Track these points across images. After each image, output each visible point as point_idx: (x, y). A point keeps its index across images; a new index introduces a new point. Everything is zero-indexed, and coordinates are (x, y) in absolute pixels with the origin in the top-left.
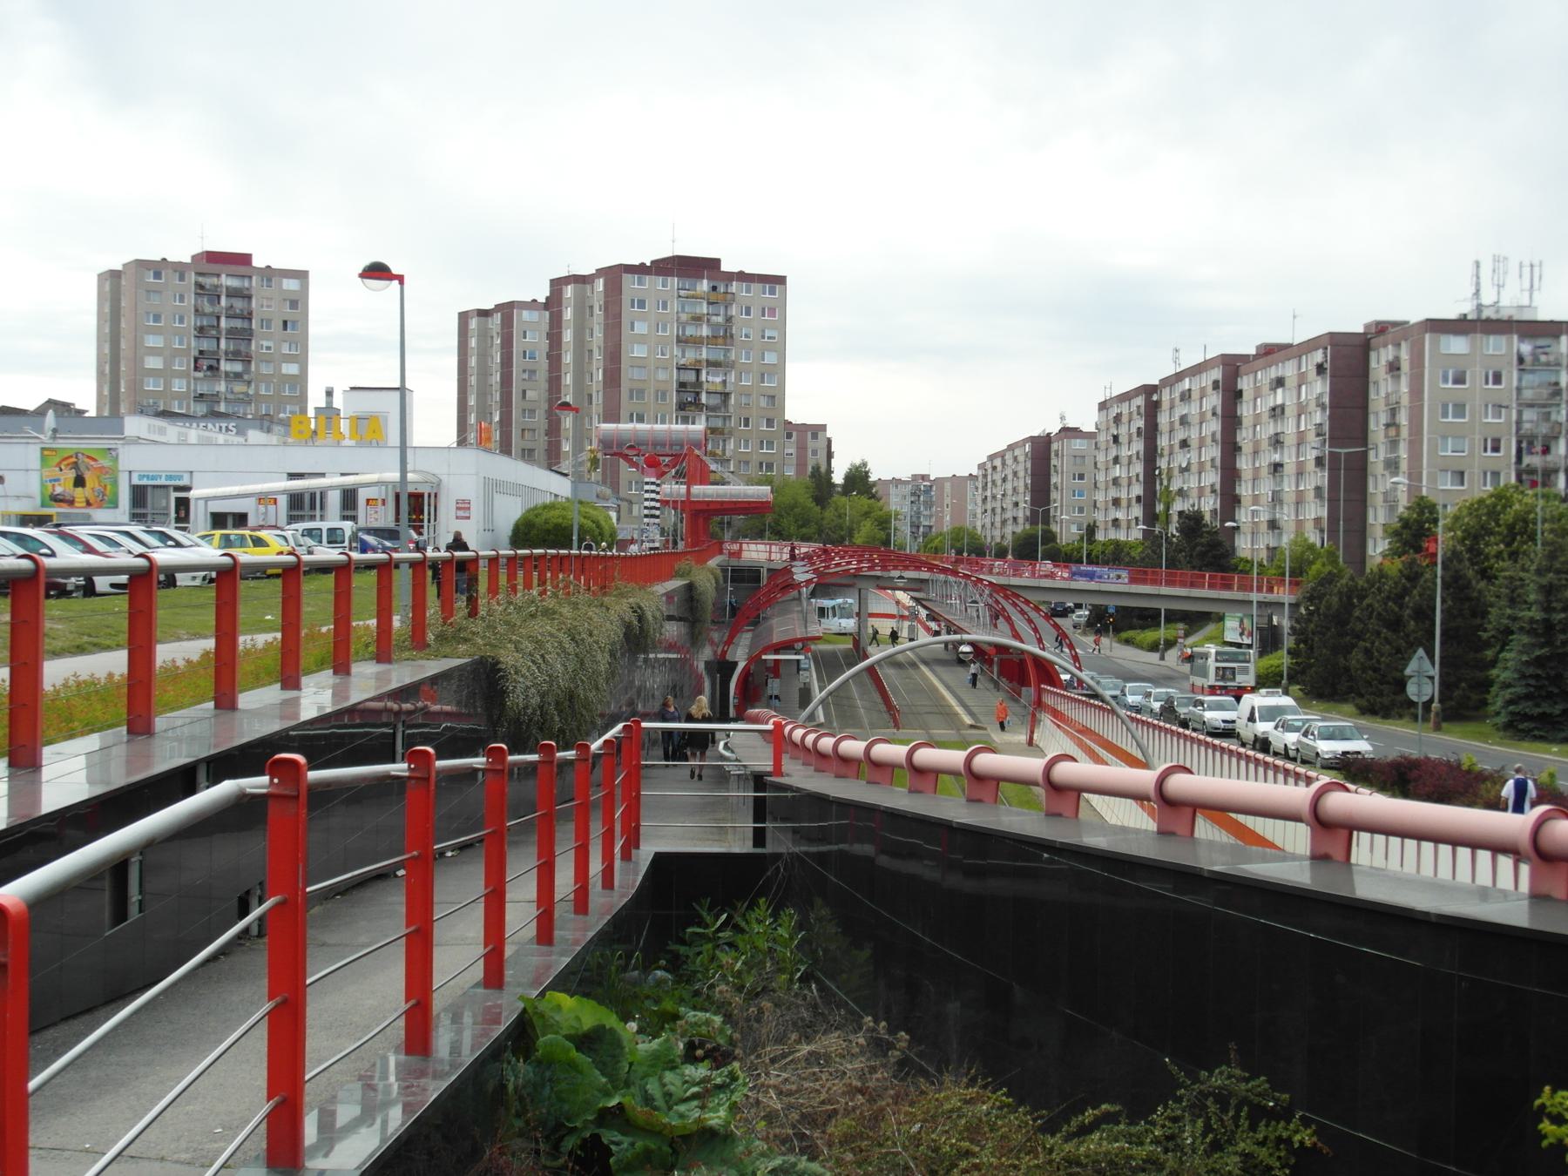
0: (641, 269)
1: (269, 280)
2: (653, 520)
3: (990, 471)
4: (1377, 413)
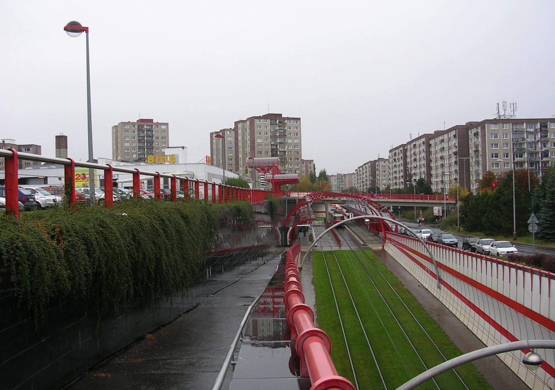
0: (259, 118)
1: (158, 126)
2: (264, 186)
3: (359, 171)
4: (472, 148)
